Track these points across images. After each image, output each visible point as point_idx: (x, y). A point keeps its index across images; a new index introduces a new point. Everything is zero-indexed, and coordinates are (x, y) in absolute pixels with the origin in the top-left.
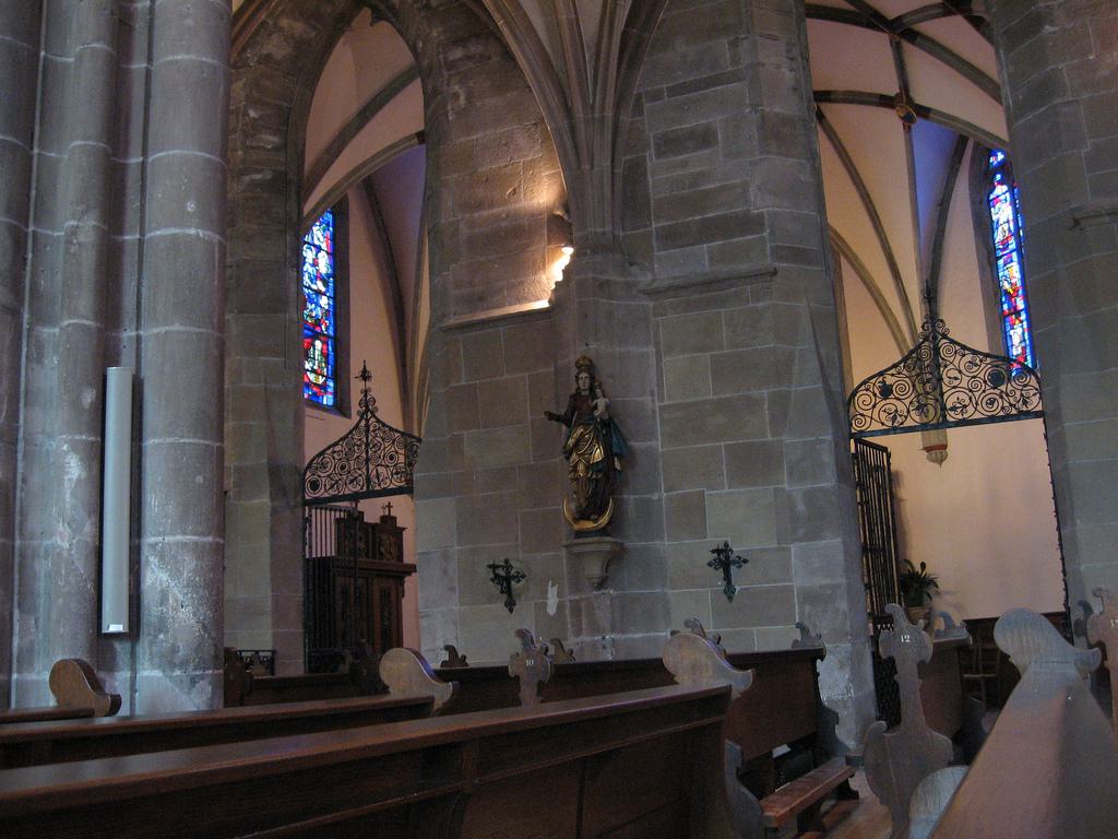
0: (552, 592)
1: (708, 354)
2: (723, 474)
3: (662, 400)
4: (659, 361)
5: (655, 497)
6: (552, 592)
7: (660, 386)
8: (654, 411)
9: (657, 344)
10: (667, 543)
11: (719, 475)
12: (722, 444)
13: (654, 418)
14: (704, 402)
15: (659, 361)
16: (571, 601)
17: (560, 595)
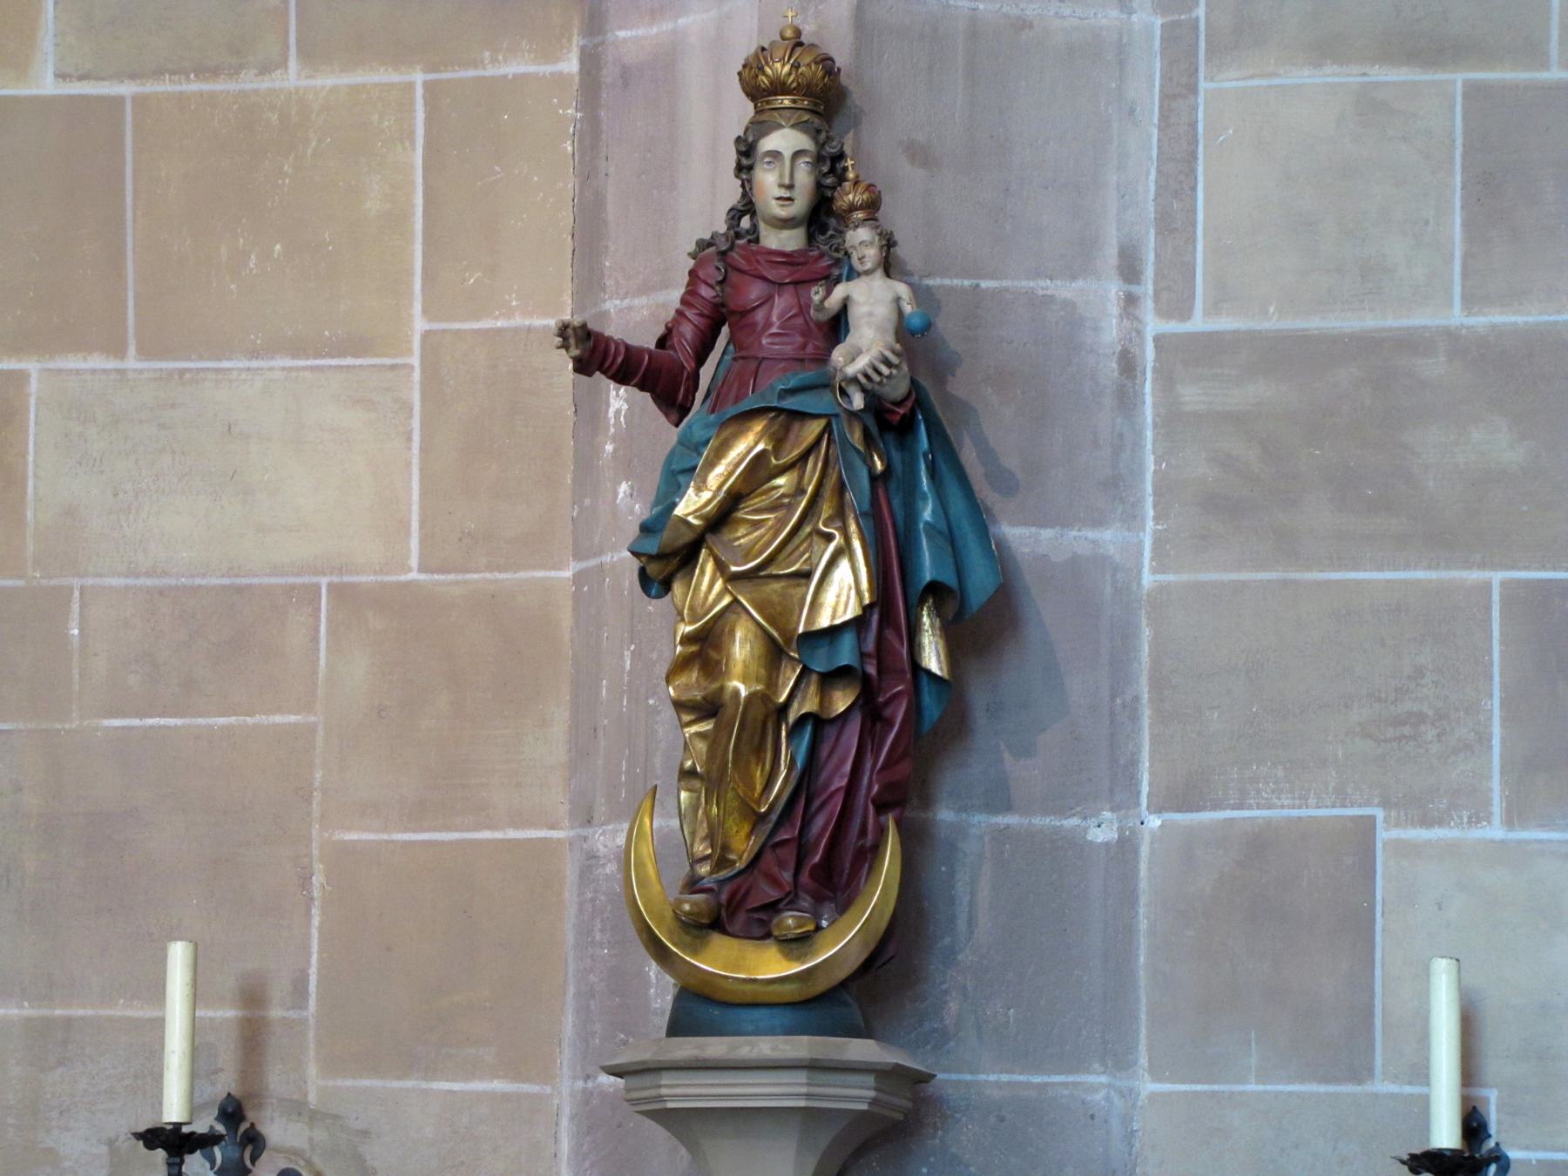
1: (1458, 79)
2: (1484, 738)
3: (1185, 313)
4: (1180, 87)
5: (1102, 832)
7: (1174, 223)
8: (1128, 364)
12: (1497, 577)
13: (1127, 400)
14: (1412, 343)
15: (1180, 87)
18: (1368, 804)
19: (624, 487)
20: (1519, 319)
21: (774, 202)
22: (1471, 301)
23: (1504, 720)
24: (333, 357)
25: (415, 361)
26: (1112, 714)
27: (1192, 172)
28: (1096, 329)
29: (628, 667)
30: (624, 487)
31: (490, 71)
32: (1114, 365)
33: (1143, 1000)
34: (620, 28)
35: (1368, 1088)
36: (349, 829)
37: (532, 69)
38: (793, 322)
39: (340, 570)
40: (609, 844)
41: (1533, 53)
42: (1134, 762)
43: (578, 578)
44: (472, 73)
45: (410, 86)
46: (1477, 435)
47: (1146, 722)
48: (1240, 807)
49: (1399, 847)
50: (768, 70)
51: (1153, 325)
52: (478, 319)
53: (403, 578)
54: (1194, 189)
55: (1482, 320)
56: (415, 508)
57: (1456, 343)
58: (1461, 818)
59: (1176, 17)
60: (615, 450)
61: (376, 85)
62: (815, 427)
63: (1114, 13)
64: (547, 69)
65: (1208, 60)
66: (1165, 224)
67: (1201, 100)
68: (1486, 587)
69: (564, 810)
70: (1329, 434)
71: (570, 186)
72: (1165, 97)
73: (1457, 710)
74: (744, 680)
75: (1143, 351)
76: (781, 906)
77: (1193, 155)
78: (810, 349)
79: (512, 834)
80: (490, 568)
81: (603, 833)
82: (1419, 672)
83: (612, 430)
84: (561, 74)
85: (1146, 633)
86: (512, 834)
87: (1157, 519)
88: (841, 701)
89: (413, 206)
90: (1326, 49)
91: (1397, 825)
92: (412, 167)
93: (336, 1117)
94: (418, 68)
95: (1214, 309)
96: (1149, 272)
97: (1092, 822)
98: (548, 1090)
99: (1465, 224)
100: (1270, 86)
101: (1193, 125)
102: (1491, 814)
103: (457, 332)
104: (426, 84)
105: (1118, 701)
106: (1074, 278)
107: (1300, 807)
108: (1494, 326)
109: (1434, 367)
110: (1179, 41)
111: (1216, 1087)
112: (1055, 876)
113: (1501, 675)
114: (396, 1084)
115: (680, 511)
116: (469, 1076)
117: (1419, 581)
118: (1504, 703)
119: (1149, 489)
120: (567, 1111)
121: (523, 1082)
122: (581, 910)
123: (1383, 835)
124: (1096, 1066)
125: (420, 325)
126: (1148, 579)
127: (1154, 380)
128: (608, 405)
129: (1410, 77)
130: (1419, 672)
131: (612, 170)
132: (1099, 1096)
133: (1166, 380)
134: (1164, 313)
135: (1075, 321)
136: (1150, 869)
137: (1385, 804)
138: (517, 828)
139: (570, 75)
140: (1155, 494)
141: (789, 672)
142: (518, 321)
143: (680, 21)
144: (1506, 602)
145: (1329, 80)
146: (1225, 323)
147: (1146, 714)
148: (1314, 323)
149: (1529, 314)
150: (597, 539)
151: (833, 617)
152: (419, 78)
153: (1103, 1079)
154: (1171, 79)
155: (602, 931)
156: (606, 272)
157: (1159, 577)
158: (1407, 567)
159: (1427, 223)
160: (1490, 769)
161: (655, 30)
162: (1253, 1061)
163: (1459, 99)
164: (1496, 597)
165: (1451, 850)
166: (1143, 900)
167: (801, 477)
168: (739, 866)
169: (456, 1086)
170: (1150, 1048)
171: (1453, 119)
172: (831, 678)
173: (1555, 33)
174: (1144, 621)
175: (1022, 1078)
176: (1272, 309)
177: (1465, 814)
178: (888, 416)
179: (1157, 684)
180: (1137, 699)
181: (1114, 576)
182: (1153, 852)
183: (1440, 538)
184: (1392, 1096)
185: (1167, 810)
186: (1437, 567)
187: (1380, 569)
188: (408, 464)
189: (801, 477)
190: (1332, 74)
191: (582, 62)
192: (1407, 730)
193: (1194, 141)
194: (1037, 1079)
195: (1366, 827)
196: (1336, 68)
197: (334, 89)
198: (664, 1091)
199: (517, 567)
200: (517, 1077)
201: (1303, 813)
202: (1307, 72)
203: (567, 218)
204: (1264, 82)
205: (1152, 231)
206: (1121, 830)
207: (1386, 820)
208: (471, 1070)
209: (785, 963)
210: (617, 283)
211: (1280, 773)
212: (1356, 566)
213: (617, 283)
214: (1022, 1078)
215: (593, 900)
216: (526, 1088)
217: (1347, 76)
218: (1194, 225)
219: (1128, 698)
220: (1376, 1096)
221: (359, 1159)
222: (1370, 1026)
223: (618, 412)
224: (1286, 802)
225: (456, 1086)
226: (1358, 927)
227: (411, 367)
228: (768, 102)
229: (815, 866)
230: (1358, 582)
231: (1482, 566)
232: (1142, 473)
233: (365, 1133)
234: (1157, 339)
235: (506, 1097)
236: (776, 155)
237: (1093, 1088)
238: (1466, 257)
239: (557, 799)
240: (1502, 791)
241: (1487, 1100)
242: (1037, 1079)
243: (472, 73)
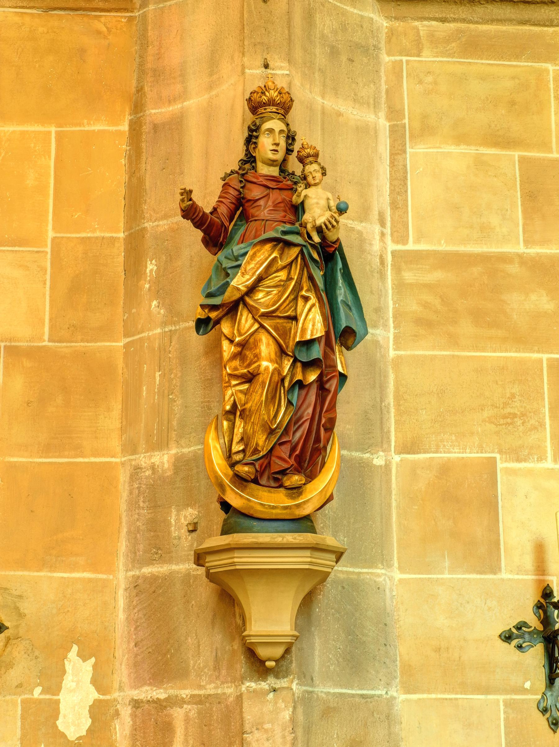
0: (78, 673)
1: (516, 154)
2: (542, 425)
3: (404, 240)
4: (397, 151)
5: (378, 460)
6: (78, 673)
7: (398, 203)
8: (382, 262)
9: (394, 113)
10: (398, 575)
11: (534, 428)
12: (545, 357)
13: (382, 276)
14: (504, 258)
15: (397, 151)
16: (136, 704)
17: (98, 682)
18: (493, 452)
19: (155, 303)
20: (548, 251)
21: (270, 152)
22: (527, 243)
23: (550, 417)
24: (10, 246)
25: (49, 250)
26: (381, 409)
27: (406, 184)
28: (371, 244)
29: (158, 383)
30: (155, 303)
31: (87, 128)
32: (378, 260)
33: (395, 537)
34: (152, 109)
35: (498, 576)
36: (12, 456)
37: (106, 128)
38: (279, 205)
39: (11, 340)
40: (148, 462)
41: (545, 146)
42: (389, 432)
43: (126, 346)
44: (78, 128)
45: (49, 133)
46: (533, 297)
47: (392, 415)
48: (436, 452)
49: (508, 471)
50: (267, 94)
51: (391, 246)
52: (79, 233)
53: (40, 344)
54: (406, 191)
55: (534, 251)
56: (47, 314)
57: (522, 259)
58: (533, 458)
59: (395, 123)
60: (150, 287)
61: (34, 132)
62: (295, 251)
63: (373, 116)
64: (114, 128)
65: (410, 141)
66: (394, 205)
67: (408, 156)
68: (541, 361)
69: (119, 449)
70: (474, 294)
71: (124, 178)
72: (391, 154)
73: (530, 412)
74: (271, 361)
75: (387, 257)
76: (288, 472)
77: (406, 178)
78: (287, 218)
79: (93, 460)
80: (82, 341)
81: (145, 457)
82: (513, 396)
83: (149, 278)
84: (120, 131)
85: (392, 377)
86: (93, 460)
87: (395, 328)
88: (312, 377)
89: (49, 183)
90: (461, 139)
91: (506, 461)
92: (49, 167)
93: (6, 589)
94: (53, 125)
95: (417, 241)
96: (389, 224)
97: (375, 456)
98: (111, 577)
99: (522, 211)
100: (438, 152)
101: (405, 166)
102: (547, 457)
103: (68, 238)
104: (57, 133)
105: (383, 404)
106: (361, 222)
107: (463, 453)
108: (538, 254)
109: (514, 269)
110: (397, 134)
111: (430, 576)
112: (360, 479)
113: (548, 398)
114: (36, 574)
115: (234, 283)
116: (72, 570)
117: (512, 357)
118: (550, 409)
119: (391, 315)
120: (123, 586)
121: (98, 573)
122: (131, 493)
123: (500, 465)
124: (380, 565)
125: (51, 234)
126: (392, 353)
127: (392, 269)
128: (146, 267)
129: (496, 152)
130: (513, 396)
131: (149, 168)
132: (381, 579)
133: (397, 269)
134: (395, 241)
135: (362, 240)
136: (396, 479)
137: (500, 452)
138: (95, 457)
139: (124, 132)
140: (393, 317)
141: (286, 362)
142: (98, 234)
143: (185, 103)
144: (550, 367)
145: (463, 151)
146: (423, 247)
147: (392, 410)
148: (462, 248)
149: (552, 249)
150: (140, 326)
151: (312, 335)
152: (53, 129)
153: (383, 571)
154: (394, 147)
155: (143, 502)
156: (145, 211)
157: (397, 352)
158: (506, 351)
159: (507, 210)
160: (546, 438)
161: (171, 109)
162: (447, 564)
163: (517, 163)
164: (545, 365)
165: (530, 472)
166: (394, 492)
167: (289, 273)
168: (261, 454)
169: (65, 575)
170: (399, 559)
171: (515, 170)
172: (308, 365)
173: (554, 140)
174: (391, 371)
175: (351, 570)
176: (443, 242)
177: (536, 457)
178: (328, 249)
179: (398, 397)
180: (389, 404)
181: (380, 350)
182: (397, 471)
183: (520, 340)
184: (510, 580)
185: (403, 453)
186: (519, 351)
187: (495, 351)
188: (44, 295)
189: (289, 273)
190: (463, 149)
191: (130, 126)
192: (509, 420)
193: (406, 172)
194: (357, 570)
195: (493, 461)
196: (465, 147)
197: (14, 132)
198: (236, 560)
199: (96, 341)
200: (96, 571)
201: (464, 455)
202: (453, 147)
203: (122, 191)
204: (435, 150)
205: (389, 208)
206: (386, 460)
207: (501, 459)
208: (73, 568)
209: (290, 501)
210: (151, 215)
211: (454, 438)
212: (484, 350)
213: (151, 215)
214: (351, 570)
215: (139, 488)
216: (100, 576)
217: (472, 150)
218: (407, 206)
219: (387, 404)
220: (503, 580)
221: (17, 608)
222: (499, 549)
223: (151, 271)
224: (457, 451)
225: (65, 575)
226: (491, 505)
227: (47, 253)
228: (265, 109)
229: (297, 455)
230: (485, 357)
231: (538, 352)
232: (388, 308)
233: (20, 597)
234: (393, 252)
235: (90, 580)
236: (271, 131)
237: (379, 575)
238: (524, 225)
239: (115, 443)
240: (551, 447)
241: (552, 581)
242: (357, 570)
243: (78, 128)
